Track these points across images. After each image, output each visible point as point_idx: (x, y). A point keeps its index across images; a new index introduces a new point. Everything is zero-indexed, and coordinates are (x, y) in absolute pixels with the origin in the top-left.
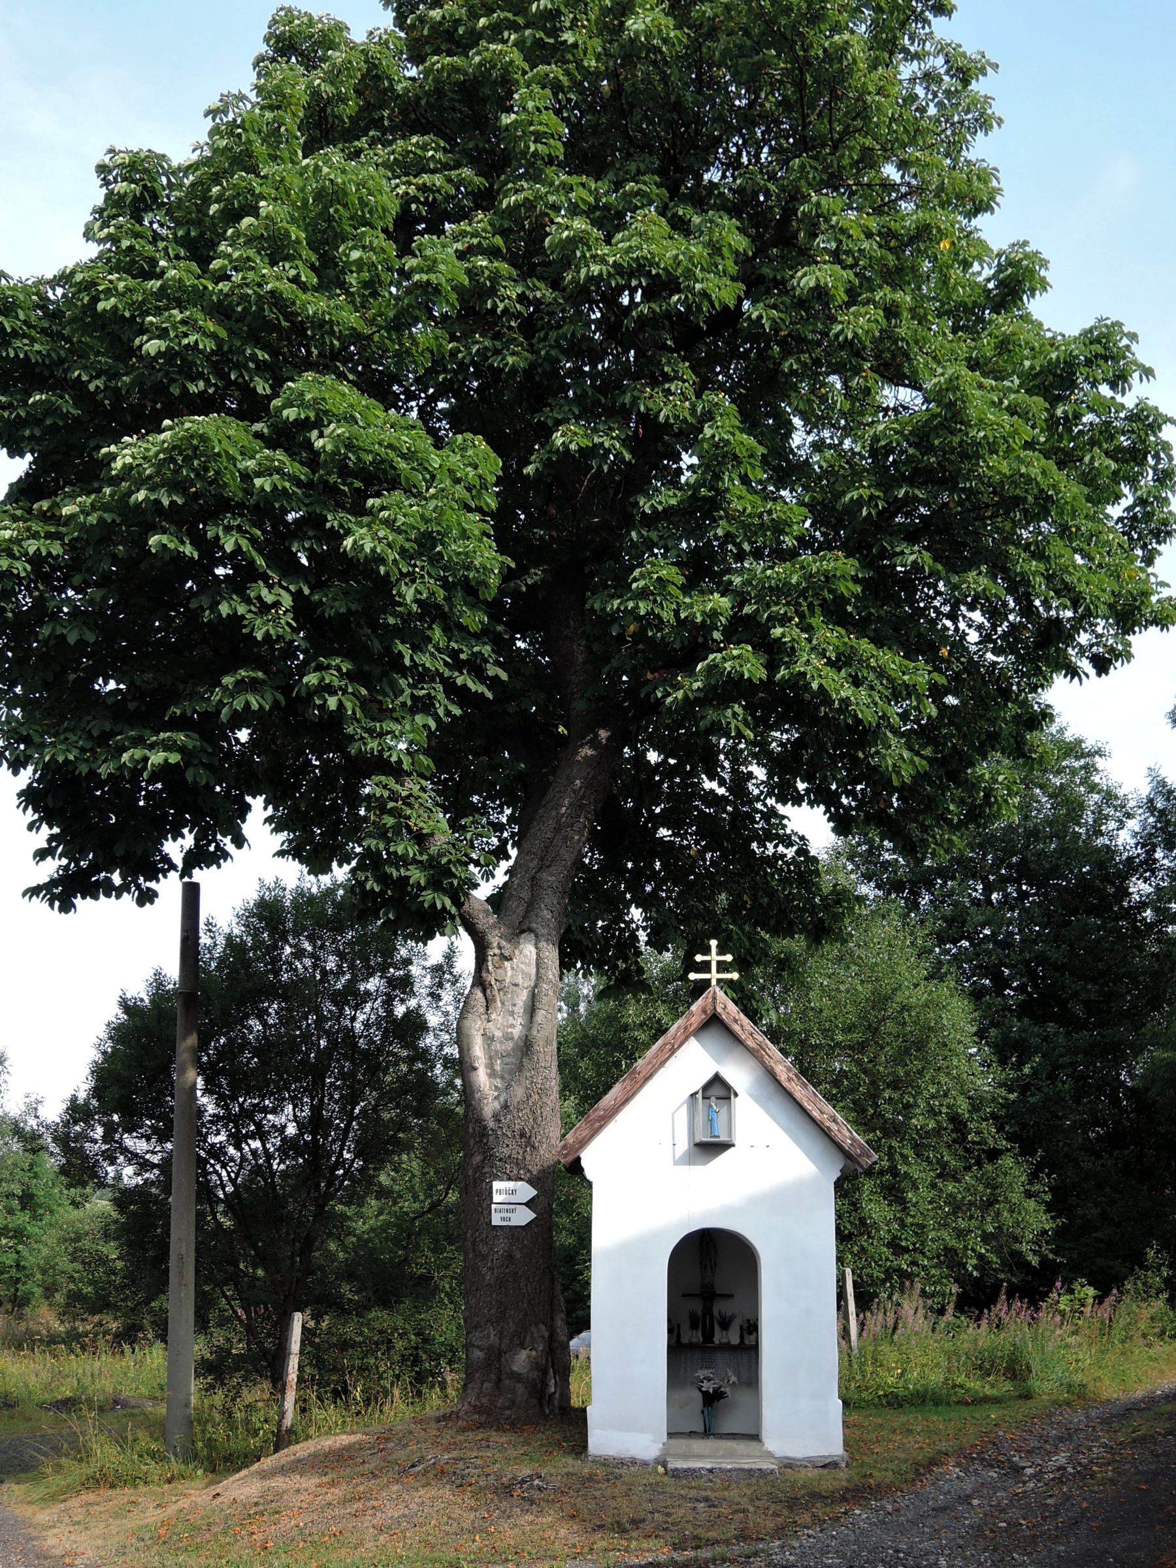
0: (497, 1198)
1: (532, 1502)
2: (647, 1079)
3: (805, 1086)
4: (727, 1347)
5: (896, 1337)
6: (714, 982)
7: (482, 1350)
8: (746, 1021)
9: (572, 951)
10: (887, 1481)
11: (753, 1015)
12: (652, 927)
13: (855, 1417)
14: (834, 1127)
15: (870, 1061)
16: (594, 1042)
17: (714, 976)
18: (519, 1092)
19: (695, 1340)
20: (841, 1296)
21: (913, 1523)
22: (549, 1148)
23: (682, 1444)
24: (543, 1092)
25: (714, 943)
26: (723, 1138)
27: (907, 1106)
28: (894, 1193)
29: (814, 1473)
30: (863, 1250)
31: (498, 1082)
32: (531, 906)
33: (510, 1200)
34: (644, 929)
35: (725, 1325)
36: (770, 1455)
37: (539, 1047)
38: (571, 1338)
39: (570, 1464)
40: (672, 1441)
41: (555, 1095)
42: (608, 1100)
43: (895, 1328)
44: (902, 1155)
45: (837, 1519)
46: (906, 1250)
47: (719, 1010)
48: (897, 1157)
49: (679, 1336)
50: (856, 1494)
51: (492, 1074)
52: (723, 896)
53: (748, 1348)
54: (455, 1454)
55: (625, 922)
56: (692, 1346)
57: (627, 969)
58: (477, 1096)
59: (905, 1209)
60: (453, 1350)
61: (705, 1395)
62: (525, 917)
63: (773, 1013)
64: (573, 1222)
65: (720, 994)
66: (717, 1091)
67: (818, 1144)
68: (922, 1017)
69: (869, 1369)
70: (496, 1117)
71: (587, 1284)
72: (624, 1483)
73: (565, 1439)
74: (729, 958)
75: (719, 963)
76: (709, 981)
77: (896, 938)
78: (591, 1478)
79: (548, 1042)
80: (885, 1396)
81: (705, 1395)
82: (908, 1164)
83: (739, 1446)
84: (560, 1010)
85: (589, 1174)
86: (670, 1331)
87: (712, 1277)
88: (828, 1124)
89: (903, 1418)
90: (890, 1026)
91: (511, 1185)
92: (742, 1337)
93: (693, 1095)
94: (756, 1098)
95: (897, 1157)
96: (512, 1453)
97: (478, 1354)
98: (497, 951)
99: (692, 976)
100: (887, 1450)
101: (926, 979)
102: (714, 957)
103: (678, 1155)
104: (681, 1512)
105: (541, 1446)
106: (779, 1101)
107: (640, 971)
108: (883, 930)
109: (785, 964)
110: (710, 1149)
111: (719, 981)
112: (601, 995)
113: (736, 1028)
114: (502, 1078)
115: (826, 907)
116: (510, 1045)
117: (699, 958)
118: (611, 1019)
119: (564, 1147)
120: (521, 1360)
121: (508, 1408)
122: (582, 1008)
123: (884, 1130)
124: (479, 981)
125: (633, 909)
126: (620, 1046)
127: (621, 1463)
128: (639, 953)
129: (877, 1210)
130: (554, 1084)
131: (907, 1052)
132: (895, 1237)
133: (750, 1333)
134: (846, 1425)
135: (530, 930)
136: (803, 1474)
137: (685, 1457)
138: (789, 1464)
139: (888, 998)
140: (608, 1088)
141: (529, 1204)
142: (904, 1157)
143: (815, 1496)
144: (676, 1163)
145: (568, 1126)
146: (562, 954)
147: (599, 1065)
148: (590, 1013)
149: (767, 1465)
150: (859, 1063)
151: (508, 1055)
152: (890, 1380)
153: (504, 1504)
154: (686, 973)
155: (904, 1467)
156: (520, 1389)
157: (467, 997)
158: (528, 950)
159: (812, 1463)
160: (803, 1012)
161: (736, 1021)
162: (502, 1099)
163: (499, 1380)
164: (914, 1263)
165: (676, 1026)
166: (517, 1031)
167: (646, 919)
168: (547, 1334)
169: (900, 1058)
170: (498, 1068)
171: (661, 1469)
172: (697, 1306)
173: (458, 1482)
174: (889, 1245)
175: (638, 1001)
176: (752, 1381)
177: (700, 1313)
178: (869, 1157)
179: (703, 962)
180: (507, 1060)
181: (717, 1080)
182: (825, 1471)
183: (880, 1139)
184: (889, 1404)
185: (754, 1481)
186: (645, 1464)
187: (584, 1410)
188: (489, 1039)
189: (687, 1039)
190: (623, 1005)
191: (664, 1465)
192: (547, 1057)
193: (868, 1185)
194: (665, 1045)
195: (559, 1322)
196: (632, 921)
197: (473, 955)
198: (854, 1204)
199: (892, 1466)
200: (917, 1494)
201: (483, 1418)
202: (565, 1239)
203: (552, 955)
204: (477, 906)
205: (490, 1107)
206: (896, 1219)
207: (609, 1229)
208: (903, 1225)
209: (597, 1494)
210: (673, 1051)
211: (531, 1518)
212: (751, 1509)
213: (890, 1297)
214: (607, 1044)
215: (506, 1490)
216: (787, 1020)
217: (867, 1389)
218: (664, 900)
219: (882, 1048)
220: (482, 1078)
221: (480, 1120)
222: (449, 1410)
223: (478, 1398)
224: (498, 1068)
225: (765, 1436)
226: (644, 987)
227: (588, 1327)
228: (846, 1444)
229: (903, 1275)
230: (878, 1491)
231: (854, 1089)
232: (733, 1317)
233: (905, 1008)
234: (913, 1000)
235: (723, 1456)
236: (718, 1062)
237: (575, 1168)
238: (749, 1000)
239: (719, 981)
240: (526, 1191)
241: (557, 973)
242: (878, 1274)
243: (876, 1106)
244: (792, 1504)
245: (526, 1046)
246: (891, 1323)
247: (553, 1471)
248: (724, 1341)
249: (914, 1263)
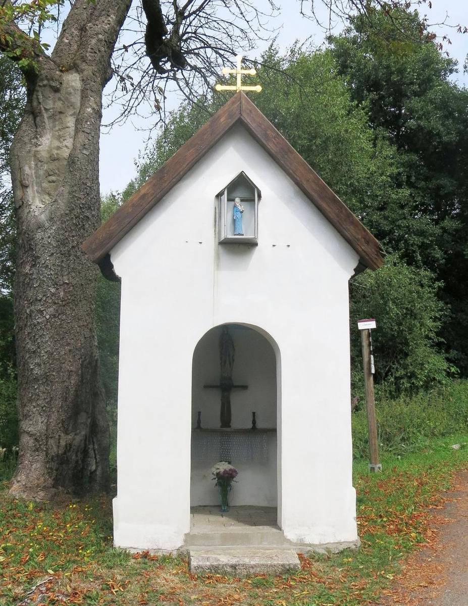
26: (248, 235)
87: (234, 376)
93: (219, 196)
110: (238, 246)
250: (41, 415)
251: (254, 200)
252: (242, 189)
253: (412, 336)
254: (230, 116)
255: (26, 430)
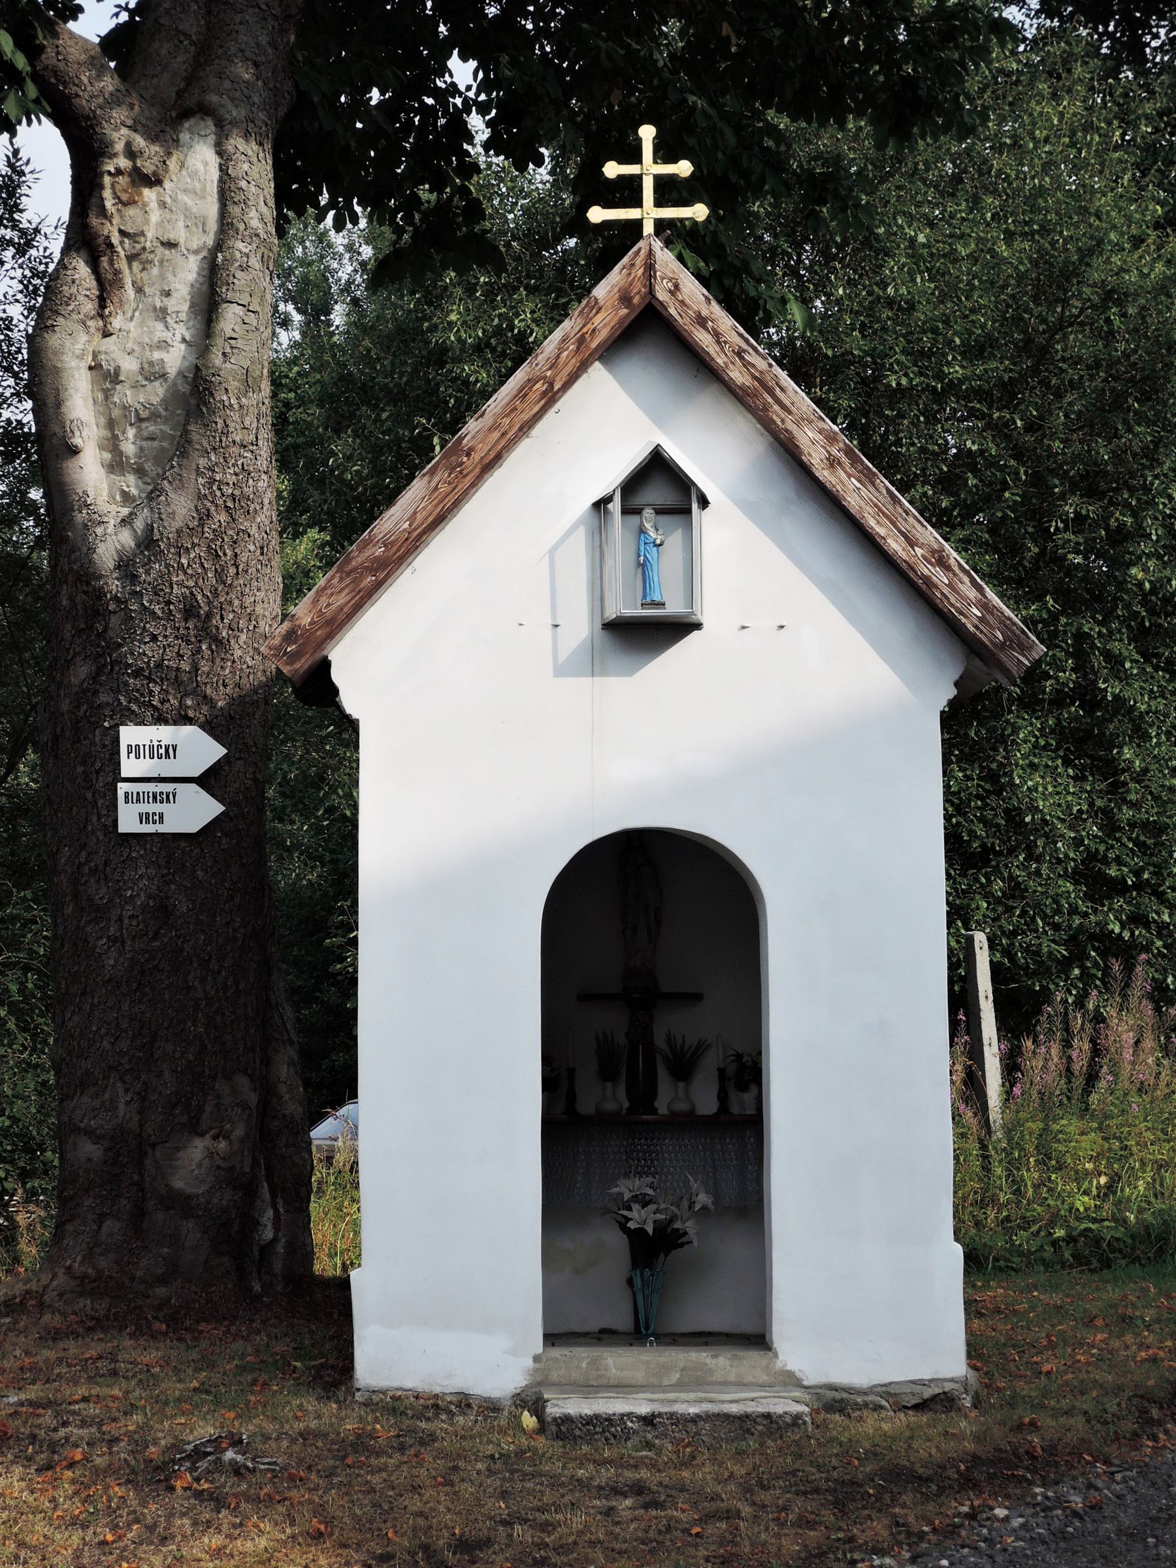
0: (129, 766)
1: (218, 1501)
2: (489, 465)
3: (870, 478)
4: (687, 1123)
5: (1094, 1098)
6: (648, 228)
7: (97, 1139)
8: (726, 322)
9: (308, 172)
10: (1072, 1438)
11: (751, 316)
12: (500, 105)
13: (997, 1292)
14: (940, 577)
15: (1030, 427)
16: (367, 394)
17: (649, 213)
18: (180, 506)
19: (610, 1106)
20: (961, 999)
21: (1133, 1536)
22: (252, 650)
23: (579, 1359)
24: (239, 505)
25: (647, 133)
26: (674, 607)
27: (1119, 536)
28: (1088, 743)
29: (894, 1423)
30: (1016, 890)
31: (131, 483)
32: (205, 53)
33: (163, 773)
34: (483, 109)
35: (683, 1067)
36: (791, 1380)
37: (229, 393)
38: (317, 1118)
39: (311, 1411)
40: (556, 1352)
41: (266, 515)
42: (394, 519)
43: (1092, 1078)
44: (1108, 655)
45: (951, 1531)
46: (1118, 887)
47: (662, 295)
48: (1097, 661)
49: (572, 1097)
50: (1000, 1469)
51: (117, 464)
52: (671, 28)
53: (740, 1127)
54: (33, 1392)
55: (436, 93)
56: (603, 1121)
57: (443, 207)
58: (81, 517)
59: (1116, 789)
60: (30, 1148)
61: (636, 1237)
62: (191, 79)
63: (795, 311)
64: (317, 830)
65: (665, 258)
66: (657, 493)
67: (899, 624)
68: (1153, 320)
69: (1031, 1176)
70: (126, 566)
71: (350, 983)
72: (441, 1454)
73: (299, 1352)
74: (684, 168)
75: (659, 180)
76: (638, 224)
77: (1088, 127)
78: (361, 1443)
79: (248, 383)
80: (1070, 1239)
81: (636, 1237)
82: (1125, 678)
83: (719, 1362)
84: (285, 323)
85: (350, 702)
86: (549, 1084)
87: (650, 957)
88: (925, 569)
89: (1112, 1293)
90: (1077, 343)
91: (164, 734)
92: (723, 1097)
93: (601, 505)
94: (750, 510)
95: (1097, 661)
96: (173, 1388)
97: (89, 1150)
98: (123, 163)
99: (597, 214)
100: (1073, 1366)
101: (1157, 226)
102: (650, 168)
103: (563, 655)
104: (578, 1521)
105: (243, 1369)
106: (807, 527)
107: (475, 210)
108: (1052, 112)
109: (826, 185)
110: (646, 633)
111: (660, 225)
112: (382, 274)
113: (703, 338)
114: (140, 472)
115: (919, 46)
116: (156, 393)
117: (612, 170)
118: (407, 336)
119: (289, 637)
120: (193, 1162)
121: (163, 1280)
122: (338, 316)
123: (1061, 594)
124: (83, 236)
125: (454, 62)
126: (431, 403)
127: (435, 1405)
128: (470, 169)
129: (1048, 791)
130: (266, 487)
131: (1118, 402)
132: (1091, 856)
133: (743, 1087)
134: (971, 1306)
135: (204, 110)
136: (870, 1424)
137: (588, 1388)
138: (837, 1402)
139: (1069, 275)
140: (391, 497)
141: (208, 781)
142: (1114, 661)
143: (900, 1477)
144: (560, 671)
145: (294, 586)
146: (283, 174)
147: (377, 450)
148: (359, 326)
149: (783, 1405)
150: (1001, 430)
151: (154, 416)
152: (1082, 1202)
153: (152, 1510)
154: (583, 208)
155: (1112, 1407)
156: (191, 1232)
157: (55, 276)
158: (199, 160)
159: (891, 1397)
160: (870, 311)
161: (702, 321)
162: (139, 524)
163: (140, 1213)
164: (1137, 919)
165: (557, 335)
166: (175, 359)
167: (484, 87)
168: (253, 1098)
169: (1099, 419)
170: (129, 448)
171: (528, 1420)
172: (615, 1023)
173: (42, 1458)
174: (1076, 877)
175: (470, 290)
176: (748, 1205)
177: (621, 1040)
178: (1024, 648)
179: (621, 178)
180: (151, 428)
181: (657, 466)
182: (924, 1418)
183: (1054, 617)
184: (1080, 1260)
185: (753, 1444)
186: (491, 1407)
187: (343, 1286)
188: (106, 377)
189: (583, 367)
190: (435, 298)
191: (537, 1407)
192: (248, 416)
193: (1027, 730)
194: (531, 382)
195: (285, 1069)
196: (453, 89)
197: (67, 173)
198: (993, 777)
199: (1086, 1403)
200: (1144, 1469)
201: (102, 1306)
202: (294, 874)
203: (256, 169)
204: (75, 54)
205: (111, 543)
206: (1094, 812)
207: (401, 826)
208: (1111, 827)
209: (375, 1480)
210: (551, 398)
211: (217, 1541)
212: (746, 1510)
213: (1080, 1003)
214: (396, 397)
215: (156, 1476)
216: (827, 328)
217: (1026, 1223)
218: (530, 40)
219: (1059, 396)
220: (90, 474)
221: (86, 575)
222: (19, 1288)
223: (89, 1258)
224: (129, 448)
225: (780, 1335)
226: (480, 251)
227: (354, 1095)
228: (974, 1352)
229: (1110, 945)
230: (1051, 1463)
231: (990, 496)
232: (701, 1048)
233: (1112, 296)
234: (1132, 277)
235: (680, 1386)
236: (659, 421)
237: (318, 686)
238: (737, 276)
239: (660, 225)
240: (199, 749)
241: (269, 213)
242: (1051, 947)
243: (1043, 535)
244: (845, 1495)
245: (196, 394)
246: (1080, 1064)
247: (270, 1427)
248: (681, 1107)
249: (1137, 919)
250: (124, 1082)
251: (688, 511)
252: (659, 489)
253: (44, 1077)
254: (625, 298)
255: (82, 1125)
